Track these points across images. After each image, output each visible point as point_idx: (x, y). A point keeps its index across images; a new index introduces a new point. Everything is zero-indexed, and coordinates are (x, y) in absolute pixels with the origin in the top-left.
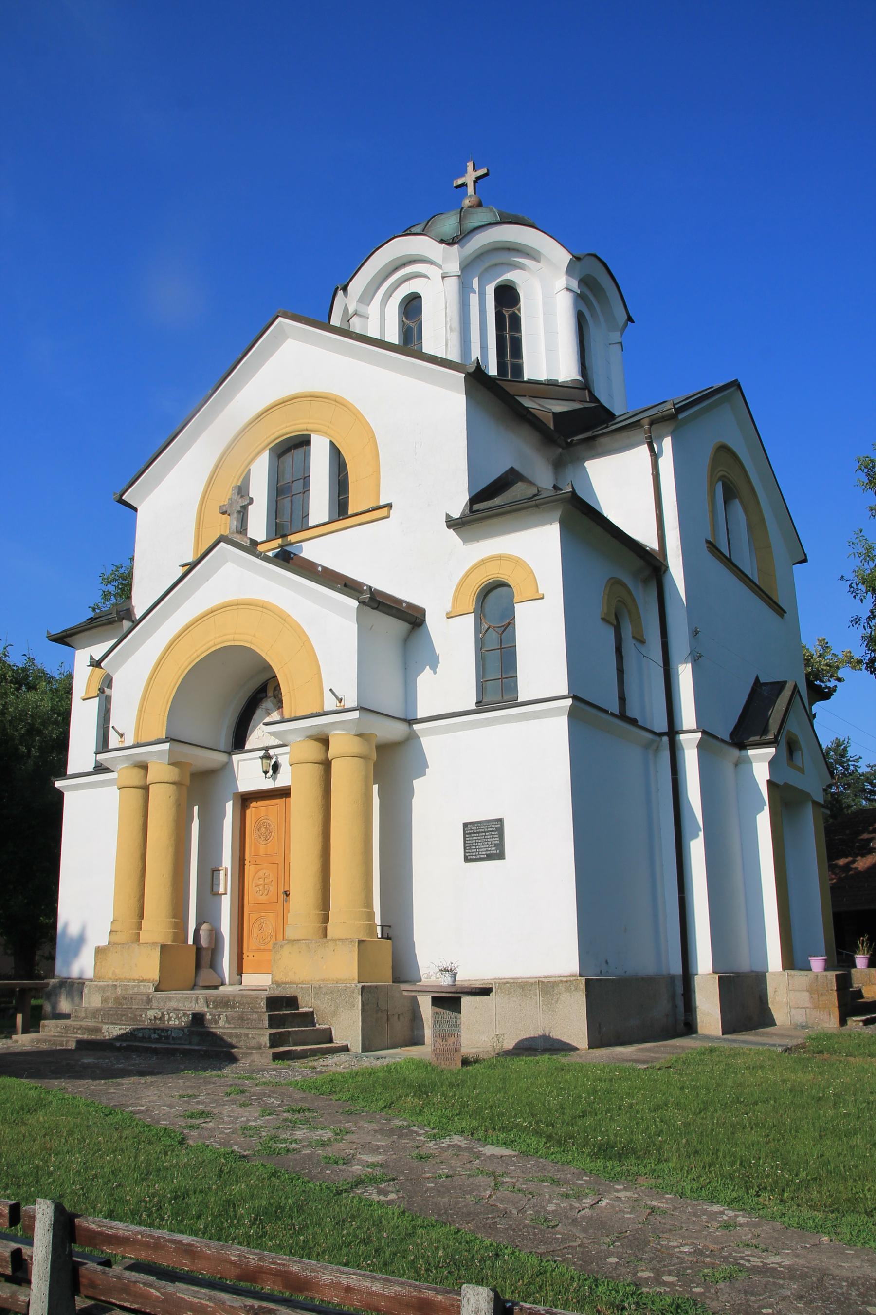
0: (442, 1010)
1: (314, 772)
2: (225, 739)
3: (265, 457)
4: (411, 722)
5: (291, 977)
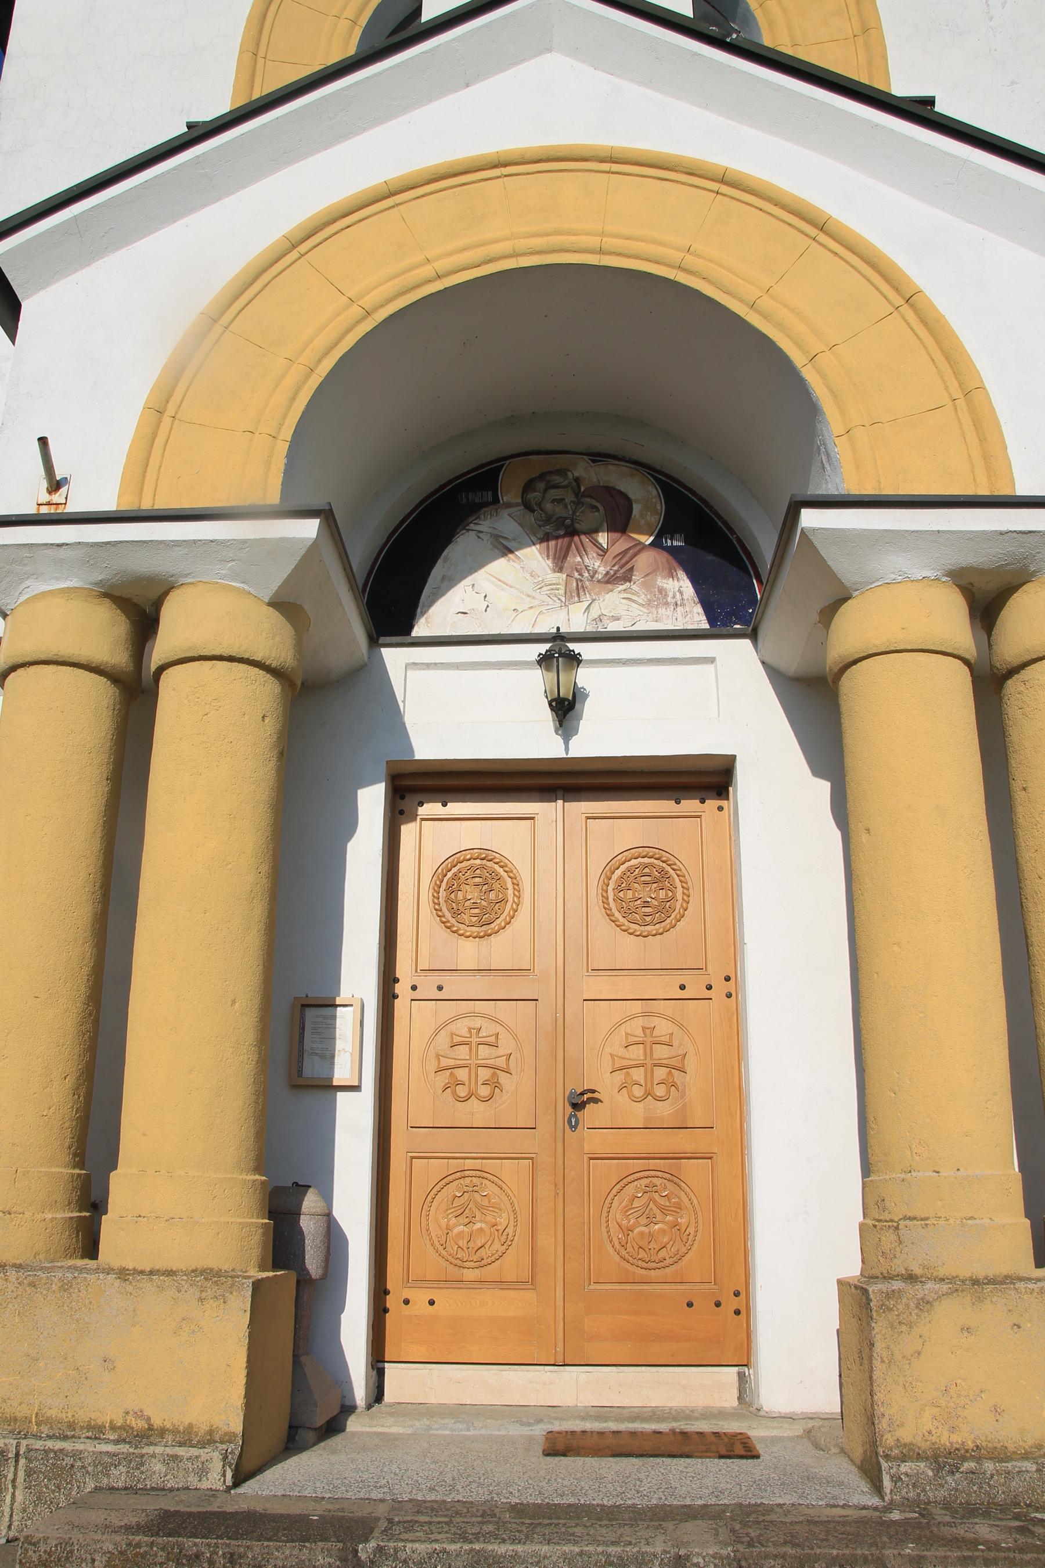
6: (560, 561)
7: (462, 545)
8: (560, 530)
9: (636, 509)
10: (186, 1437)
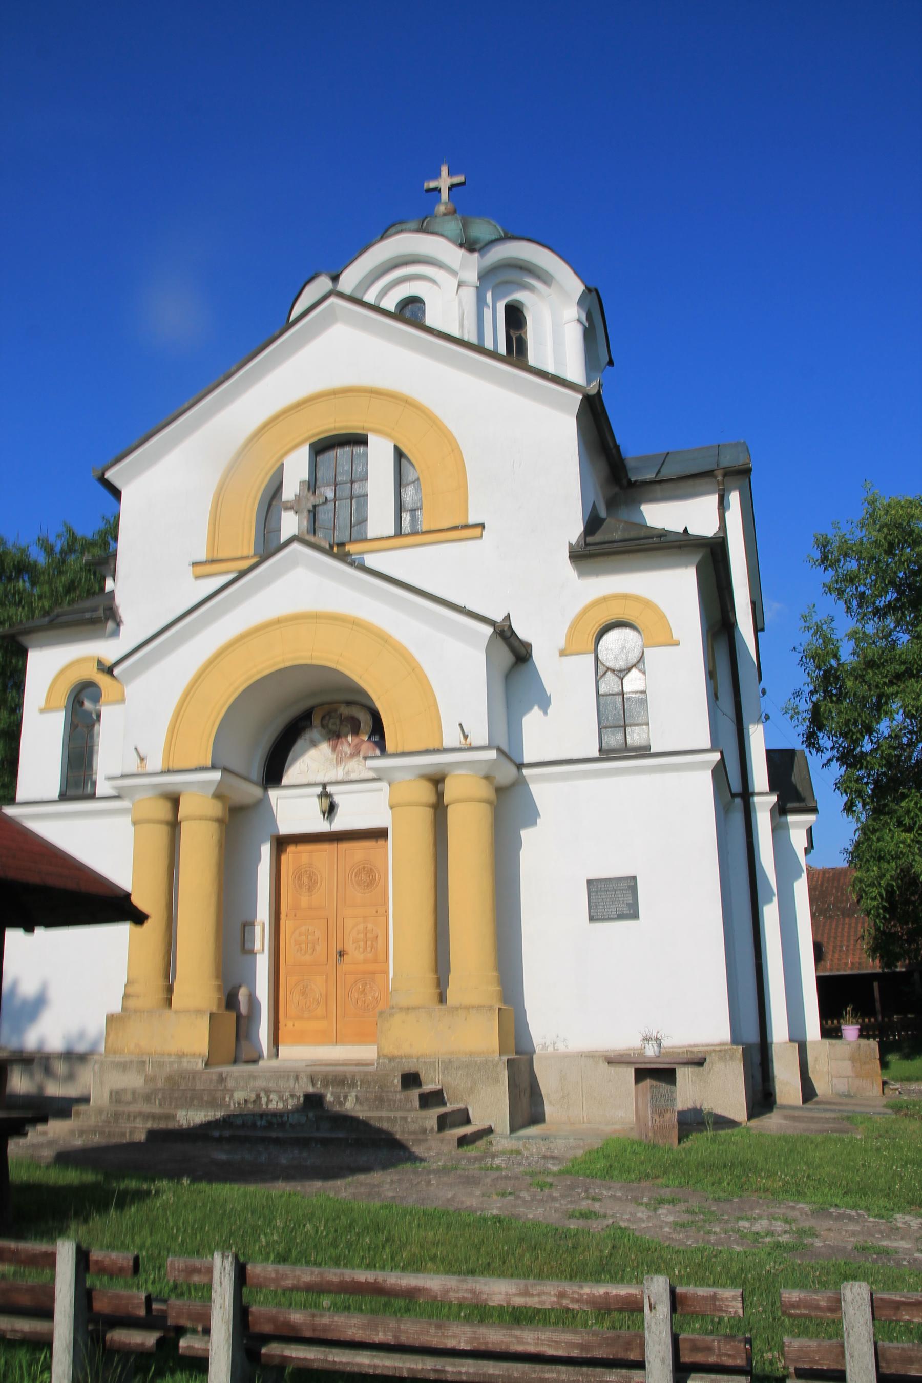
0: (658, 1084)
1: (422, 818)
2: (256, 770)
3: (303, 454)
4: (520, 766)
5: (405, 1049)
6: (334, 749)
7: (300, 744)
8: (334, 736)
9: (362, 725)
10: (194, 1055)
